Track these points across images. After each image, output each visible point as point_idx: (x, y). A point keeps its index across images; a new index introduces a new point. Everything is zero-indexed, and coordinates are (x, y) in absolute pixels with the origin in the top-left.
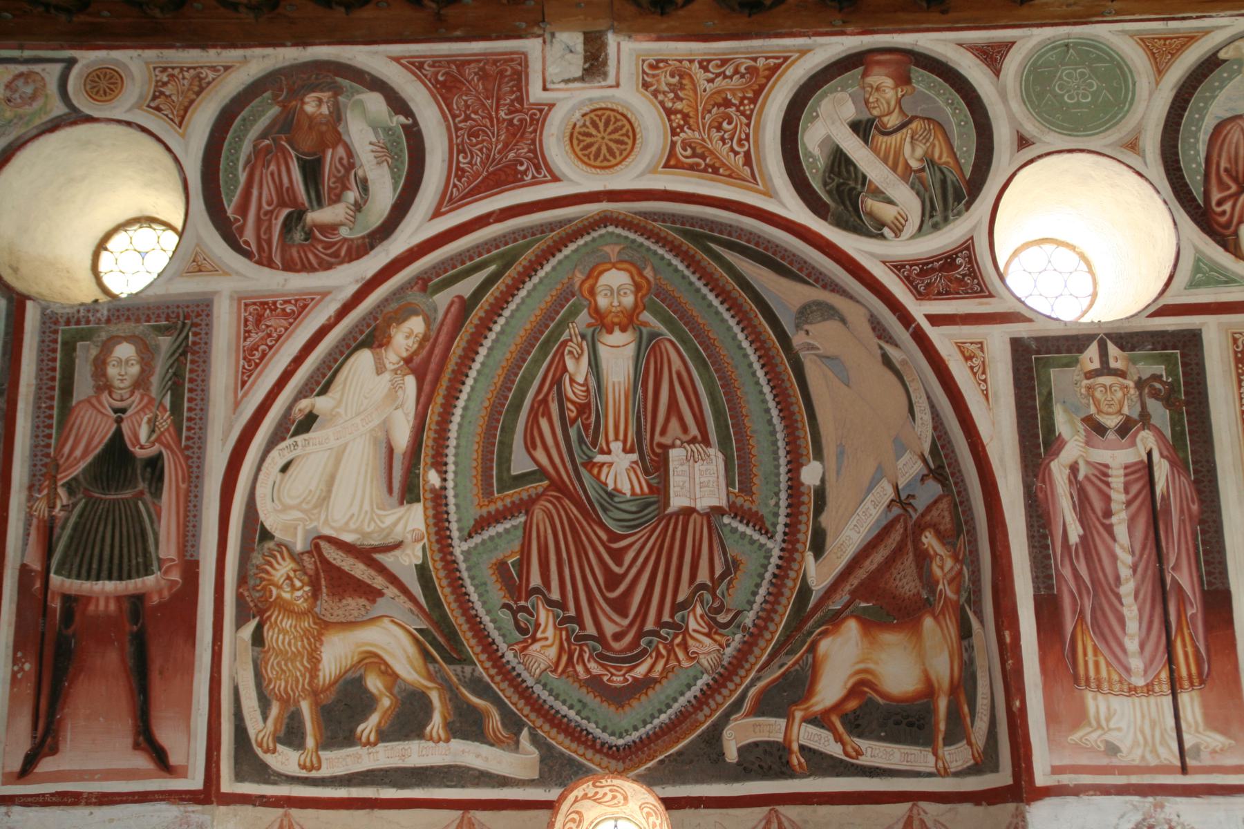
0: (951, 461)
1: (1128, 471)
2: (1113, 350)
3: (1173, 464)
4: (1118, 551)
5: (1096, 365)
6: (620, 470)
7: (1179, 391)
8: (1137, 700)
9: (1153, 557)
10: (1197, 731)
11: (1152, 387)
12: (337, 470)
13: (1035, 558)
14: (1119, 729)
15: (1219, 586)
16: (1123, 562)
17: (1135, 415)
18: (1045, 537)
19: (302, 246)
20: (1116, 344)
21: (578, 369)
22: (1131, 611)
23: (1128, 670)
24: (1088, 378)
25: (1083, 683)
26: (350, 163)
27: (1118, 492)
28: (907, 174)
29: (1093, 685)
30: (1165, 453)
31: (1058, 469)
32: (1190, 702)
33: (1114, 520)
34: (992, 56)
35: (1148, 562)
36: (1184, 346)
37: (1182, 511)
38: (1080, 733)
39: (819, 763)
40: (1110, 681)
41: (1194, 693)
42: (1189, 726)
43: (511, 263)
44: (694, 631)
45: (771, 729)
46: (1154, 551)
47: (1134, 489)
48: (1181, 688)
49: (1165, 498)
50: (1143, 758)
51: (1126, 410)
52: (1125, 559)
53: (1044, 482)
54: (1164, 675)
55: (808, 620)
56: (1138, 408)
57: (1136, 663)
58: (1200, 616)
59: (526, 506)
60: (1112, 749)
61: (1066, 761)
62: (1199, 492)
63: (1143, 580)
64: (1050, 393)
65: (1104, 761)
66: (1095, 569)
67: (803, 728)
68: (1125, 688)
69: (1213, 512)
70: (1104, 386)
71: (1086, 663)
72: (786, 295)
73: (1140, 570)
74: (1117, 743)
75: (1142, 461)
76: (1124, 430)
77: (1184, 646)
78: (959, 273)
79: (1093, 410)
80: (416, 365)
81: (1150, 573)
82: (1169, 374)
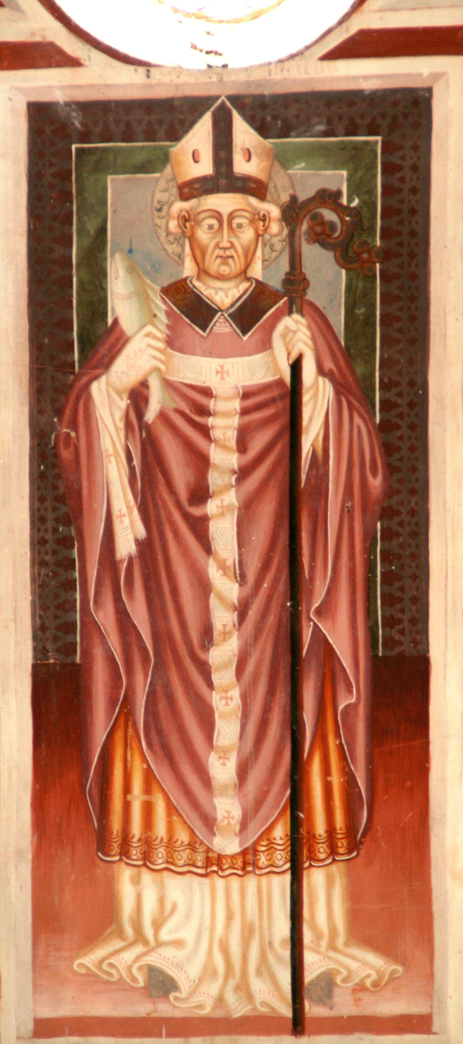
1: (250, 402)
2: (243, 133)
3: (340, 389)
4: (214, 573)
5: (205, 167)
7: (373, 228)
8: (220, 883)
9: (282, 587)
10: (332, 946)
11: (317, 219)
13: (43, 586)
14: (178, 944)
15: (407, 648)
16: (221, 598)
17: (275, 282)
18: (67, 542)
20: (251, 120)
22: (226, 700)
23: (209, 822)
24: (184, 197)
25: (116, 847)
27: (225, 447)
29: (135, 853)
30: (329, 365)
31: (107, 399)
32: (326, 889)
33: (212, 507)
35: (269, 598)
36: (394, 125)
37: (349, 491)
38: (99, 953)
40: (170, 844)
41: (335, 868)
42: (318, 936)
46: (284, 577)
47: (258, 443)
48: (312, 857)
49: (319, 462)
50: (220, 1001)
51: (257, 271)
52: (226, 588)
53: (74, 425)
54: (280, 833)
56: (284, 266)
57: (227, 808)
58: (362, 710)
60: (161, 984)
61: (66, 1010)
62: (388, 449)
63: (256, 638)
64: (103, 230)
65: (142, 1009)
66: (164, 610)
68: (200, 859)
69: (413, 492)
70: (218, 216)
71: (127, 806)
73: (252, 614)
74: (171, 972)
75: (280, 383)
76: (251, 313)
77: (326, 771)
79: (189, 268)
81: (271, 619)
82: (356, 188)
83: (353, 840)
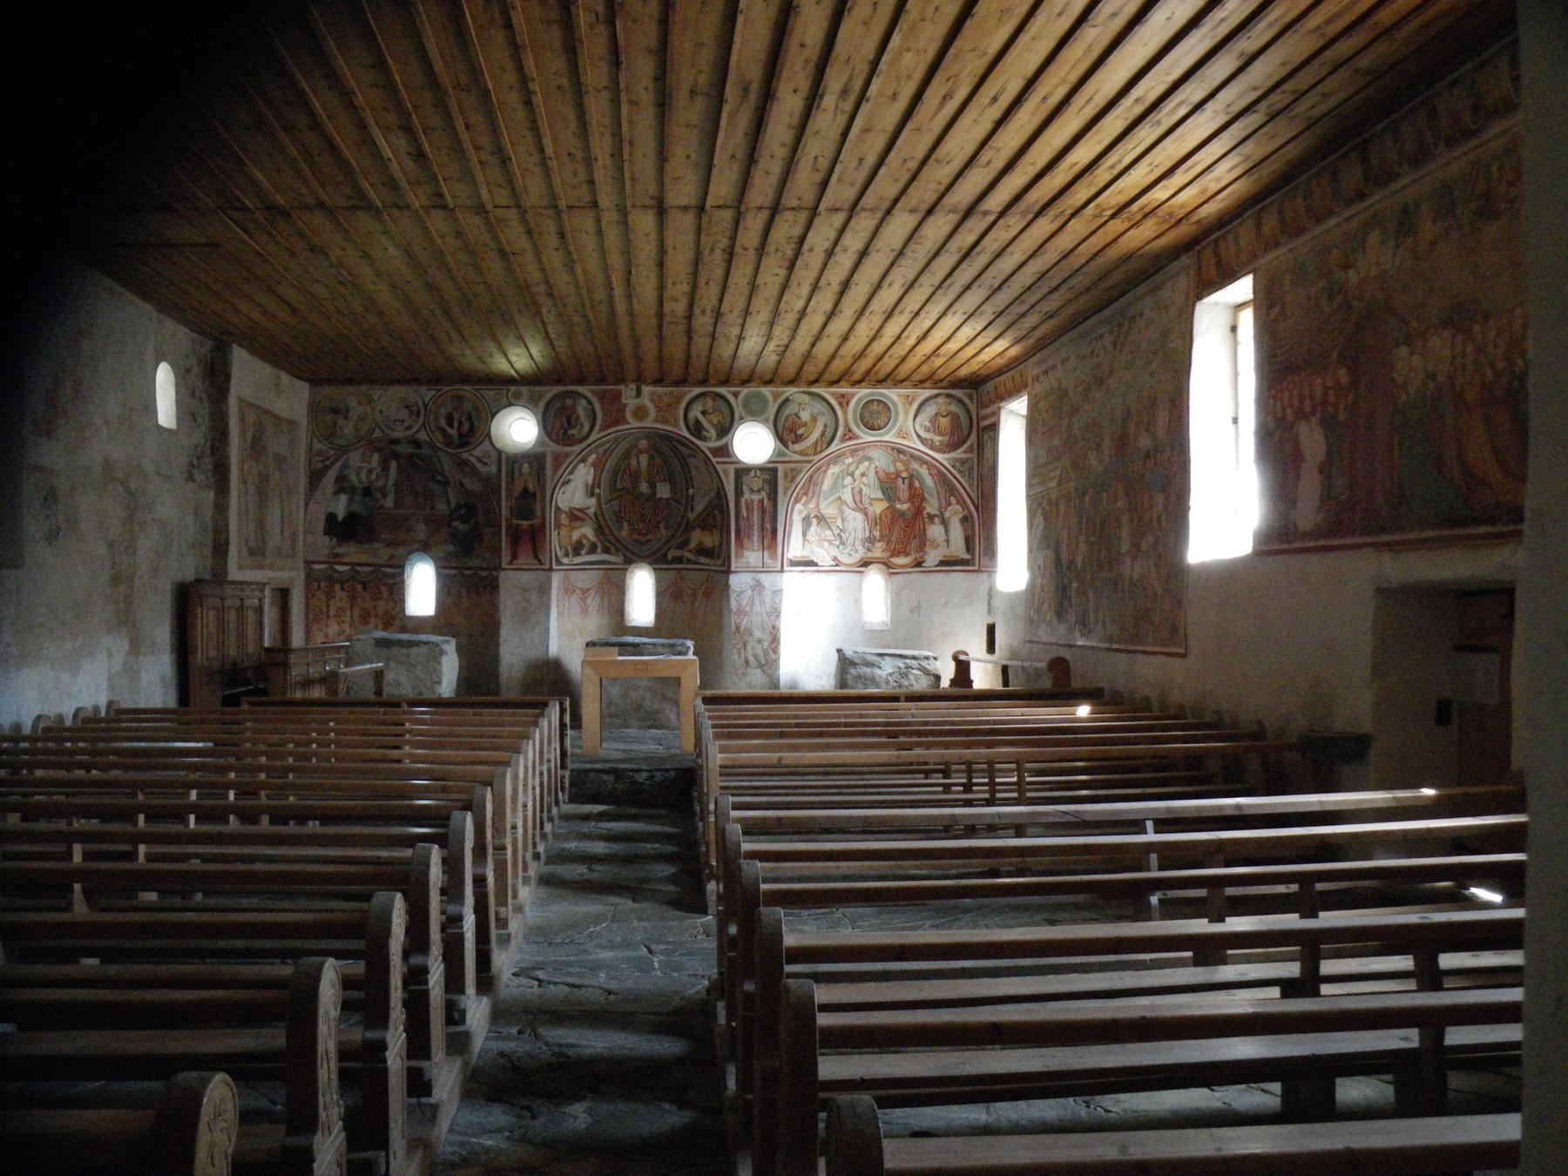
0: (721, 495)
6: (644, 487)
12: (574, 491)
19: (571, 441)
21: (634, 462)
26: (578, 418)
28: (714, 426)
34: (736, 395)
39: (689, 561)
43: (617, 441)
44: (754, 829)
45: (678, 553)
55: (689, 527)
59: (620, 497)
67: (689, 746)
72: (685, 451)
78: (725, 451)
80: (593, 465)
83: (769, 547)
